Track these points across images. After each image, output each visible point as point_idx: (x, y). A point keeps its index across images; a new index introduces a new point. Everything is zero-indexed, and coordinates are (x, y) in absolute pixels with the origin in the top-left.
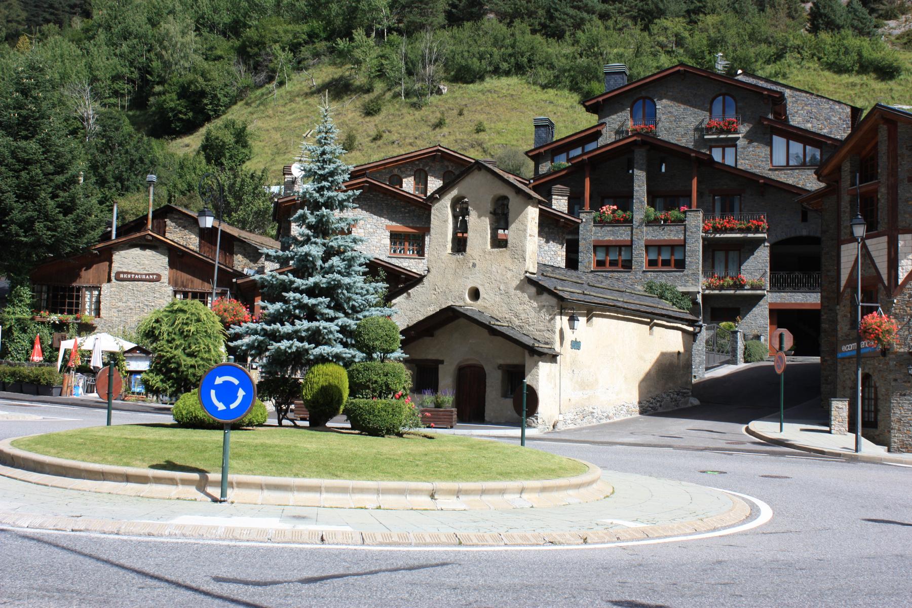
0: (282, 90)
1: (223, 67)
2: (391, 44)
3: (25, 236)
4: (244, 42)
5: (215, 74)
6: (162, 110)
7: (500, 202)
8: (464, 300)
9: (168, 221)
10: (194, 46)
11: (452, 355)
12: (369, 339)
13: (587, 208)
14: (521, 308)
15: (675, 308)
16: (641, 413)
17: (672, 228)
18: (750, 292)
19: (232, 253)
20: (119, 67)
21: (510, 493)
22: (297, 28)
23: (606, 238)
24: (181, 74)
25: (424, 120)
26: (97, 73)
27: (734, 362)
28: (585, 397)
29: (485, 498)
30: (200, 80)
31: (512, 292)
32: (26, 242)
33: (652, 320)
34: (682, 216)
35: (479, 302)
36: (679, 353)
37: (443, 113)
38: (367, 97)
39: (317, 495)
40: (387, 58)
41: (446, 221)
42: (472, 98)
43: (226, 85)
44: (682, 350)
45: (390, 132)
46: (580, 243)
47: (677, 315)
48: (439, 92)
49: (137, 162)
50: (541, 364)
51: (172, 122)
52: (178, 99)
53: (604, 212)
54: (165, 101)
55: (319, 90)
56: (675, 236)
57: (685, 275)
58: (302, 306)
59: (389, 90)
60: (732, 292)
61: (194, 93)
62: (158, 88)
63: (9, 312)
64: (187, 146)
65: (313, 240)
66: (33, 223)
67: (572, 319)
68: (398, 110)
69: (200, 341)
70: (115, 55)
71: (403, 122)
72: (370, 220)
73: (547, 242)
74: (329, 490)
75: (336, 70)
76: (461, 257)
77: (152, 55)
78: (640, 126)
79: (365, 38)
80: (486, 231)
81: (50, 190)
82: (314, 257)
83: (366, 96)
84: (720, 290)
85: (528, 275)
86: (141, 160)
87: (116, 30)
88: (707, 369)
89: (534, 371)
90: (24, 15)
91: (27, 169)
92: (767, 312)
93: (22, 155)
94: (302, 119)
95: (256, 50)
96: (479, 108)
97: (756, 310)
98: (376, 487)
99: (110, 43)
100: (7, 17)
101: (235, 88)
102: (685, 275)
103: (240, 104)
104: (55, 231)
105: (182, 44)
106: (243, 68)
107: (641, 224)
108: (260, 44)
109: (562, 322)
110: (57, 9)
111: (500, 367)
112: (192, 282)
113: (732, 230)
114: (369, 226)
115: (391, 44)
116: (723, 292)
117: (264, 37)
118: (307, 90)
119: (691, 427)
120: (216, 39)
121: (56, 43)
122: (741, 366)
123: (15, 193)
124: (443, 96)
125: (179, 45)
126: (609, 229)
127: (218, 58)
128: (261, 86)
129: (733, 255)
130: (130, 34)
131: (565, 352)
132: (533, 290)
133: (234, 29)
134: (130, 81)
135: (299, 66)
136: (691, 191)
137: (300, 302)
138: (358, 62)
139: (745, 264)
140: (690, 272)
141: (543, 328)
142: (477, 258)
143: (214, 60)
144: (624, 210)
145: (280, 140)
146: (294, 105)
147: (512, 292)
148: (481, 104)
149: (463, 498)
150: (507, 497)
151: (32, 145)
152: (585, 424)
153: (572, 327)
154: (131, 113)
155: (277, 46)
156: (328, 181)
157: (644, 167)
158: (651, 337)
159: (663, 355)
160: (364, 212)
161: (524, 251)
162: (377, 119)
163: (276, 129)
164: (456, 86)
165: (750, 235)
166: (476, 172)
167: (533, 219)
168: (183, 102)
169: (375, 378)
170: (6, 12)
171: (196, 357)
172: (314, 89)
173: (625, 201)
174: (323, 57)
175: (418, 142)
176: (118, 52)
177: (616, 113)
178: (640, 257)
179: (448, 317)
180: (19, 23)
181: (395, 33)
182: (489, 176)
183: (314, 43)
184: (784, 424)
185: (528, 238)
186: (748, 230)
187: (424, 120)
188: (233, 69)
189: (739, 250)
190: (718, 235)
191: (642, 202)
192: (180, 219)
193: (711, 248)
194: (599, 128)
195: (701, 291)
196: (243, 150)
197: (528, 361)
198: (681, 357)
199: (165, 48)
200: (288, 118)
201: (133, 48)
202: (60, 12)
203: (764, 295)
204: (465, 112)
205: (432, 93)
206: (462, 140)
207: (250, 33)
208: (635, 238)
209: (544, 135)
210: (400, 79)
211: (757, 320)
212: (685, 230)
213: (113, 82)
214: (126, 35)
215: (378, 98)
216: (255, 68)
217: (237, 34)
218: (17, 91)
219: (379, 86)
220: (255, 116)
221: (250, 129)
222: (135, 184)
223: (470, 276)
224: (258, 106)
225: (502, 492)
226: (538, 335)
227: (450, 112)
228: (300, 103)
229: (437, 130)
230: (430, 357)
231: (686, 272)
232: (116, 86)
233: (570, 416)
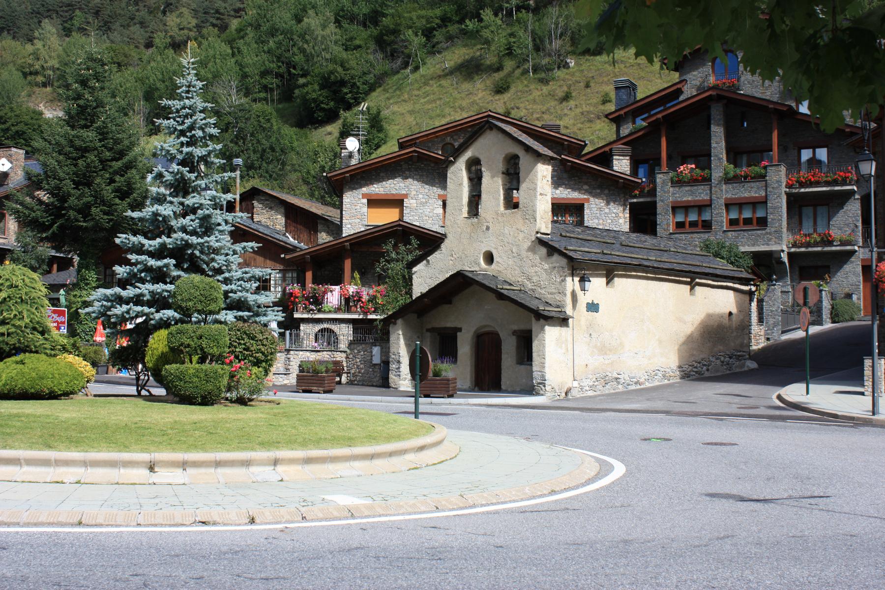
0: (417, 75)
1: (361, 56)
2: (518, 21)
3: (85, 221)
4: (381, 30)
5: (353, 63)
6: (305, 101)
7: (512, 161)
8: (479, 264)
9: (255, 203)
10: (334, 38)
11: (468, 322)
12: (182, 300)
13: (665, 168)
14: (533, 270)
15: (730, 267)
16: (682, 378)
17: (753, 184)
18: (838, 248)
19: (316, 231)
20: (267, 63)
21: (211, 462)
22: (430, 13)
23: (685, 199)
24: (322, 66)
25: (551, 95)
26: (247, 70)
27: (819, 322)
28: (607, 362)
29: (220, 470)
30: (340, 69)
31: (524, 254)
32: (86, 228)
33: (693, 280)
34: (763, 171)
36: (730, 314)
37: (569, 87)
38: (497, 76)
39: (17, 468)
40: (515, 36)
41: (461, 184)
42: (599, 70)
43: (364, 74)
44: (734, 311)
45: (518, 108)
46: (658, 205)
47: (731, 274)
48: (566, 66)
49: (268, 150)
50: (547, 328)
51: (314, 112)
52: (320, 90)
53: (681, 172)
54: (307, 92)
55: (451, 72)
56: (756, 192)
57: (767, 233)
58: (148, 269)
59: (518, 67)
60: (819, 249)
61: (335, 83)
62: (302, 81)
63: (75, 296)
64: (330, 134)
65: (169, 199)
66: (90, 208)
67: (583, 280)
68: (526, 86)
69: (13, 308)
70: (264, 51)
71: (531, 97)
72: (422, 190)
73: (608, 204)
74: (30, 462)
75: (468, 52)
76: (476, 220)
77: (295, 49)
78: (725, 81)
79: (493, 18)
80: (498, 192)
81: (107, 176)
82: (165, 217)
83: (496, 75)
84: (807, 247)
85: (539, 235)
86: (272, 149)
87: (264, 28)
88: (783, 332)
89: (540, 336)
90: (194, 22)
91: (84, 157)
92: (860, 269)
93: (78, 143)
94: (434, 101)
95: (392, 38)
96: (605, 79)
97: (847, 267)
98: (82, 459)
99: (260, 41)
100: (179, 25)
101: (372, 75)
102: (767, 233)
103: (378, 90)
104: (113, 215)
105: (323, 36)
106: (380, 56)
107: (720, 182)
108: (396, 32)
109: (572, 283)
110: (223, 14)
111: (514, 333)
112: (255, 260)
113: (818, 184)
114: (421, 196)
115: (518, 21)
116: (810, 249)
117: (399, 25)
118: (440, 73)
119: (722, 391)
120: (355, 29)
121: (209, 44)
122: (828, 326)
123: (73, 181)
124: (571, 70)
125: (320, 38)
126: (687, 188)
127: (358, 47)
128: (398, 72)
129: (822, 211)
130: (277, 30)
131: (579, 316)
132: (543, 251)
133: (374, 18)
134: (278, 75)
135: (433, 50)
136: (771, 145)
137: (146, 265)
138: (487, 42)
139: (835, 219)
140: (773, 230)
141: (554, 291)
142: (491, 220)
143: (353, 50)
144: (703, 169)
145: (414, 123)
146: (428, 88)
147: (524, 254)
148: (608, 75)
149: (191, 471)
150: (253, 469)
151: (90, 135)
152: (609, 389)
153: (583, 289)
154: (280, 106)
155: (410, 32)
156: (187, 137)
157: (722, 122)
158: (692, 297)
159: (709, 316)
160: (415, 182)
161: (535, 211)
162: (506, 96)
163: (411, 112)
164: (583, 59)
165: (837, 188)
166: (488, 132)
167: (545, 177)
168: (325, 92)
169: (188, 341)
170: (178, 21)
171: (8, 323)
172: (447, 71)
173: (703, 158)
174: (456, 40)
175: (545, 116)
176: (266, 48)
177: (697, 69)
178: (720, 217)
179: (459, 284)
180: (190, 30)
181: (524, 11)
182: (500, 136)
183: (446, 26)
184: (812, 387)
185: (539, 197)
186: (835, 182)
187: (551, 95)
188: (371, 57)
189: (828, 205)
190: (802, 190)
191: (720, 159)
192: (267, 200)
193: (798, 205)
194: (679, 86)
195: (785, 248)
196: (379, 135)
197: (535, 328)
198: (734, 318)
199: (307, 42)
200: (422, 101)
201: (280, 43)
202: (225, 17)
203: (855, 252)
204: (592, 84)
205: (559, 68)
206: (588, 112)
207: (385, 21)
208: (714, 197)
209: (624, 97)
210: (528, 56)
211: (850, 277)
212: (766, 186)
213: (262, 78)
214: (273, 32)
215: (509, 75)
216: (392, 55)
217: (376, 23)
218: (76, 82)
219: (509, 64)
220: (391, 101)
221: (385, 113)
222: (267, 172)
223: (484, 240)
224: (395, 91)
225: (247, 463)
226: (549, 298)
227: (577, 85)
228: (434, 86)
229: (564, 103)
230: (449, 325)
231: (768, 230)
232: (264, 81)
233: (586, 383)
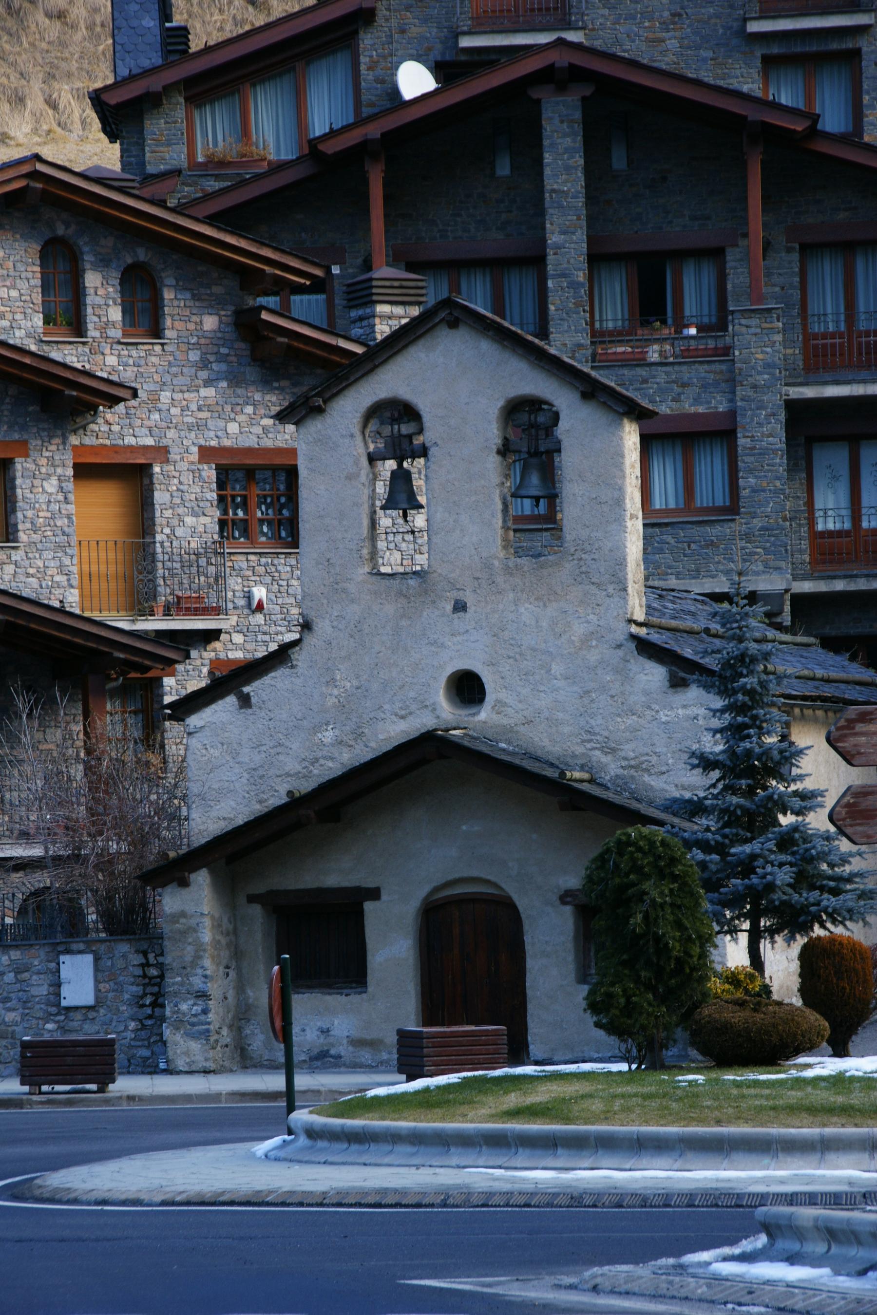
35: (485, 714)
56: (697, 401)
85: (634, 629)
111: (566, 897)
140: (757, 523)
230: (332, 881)
